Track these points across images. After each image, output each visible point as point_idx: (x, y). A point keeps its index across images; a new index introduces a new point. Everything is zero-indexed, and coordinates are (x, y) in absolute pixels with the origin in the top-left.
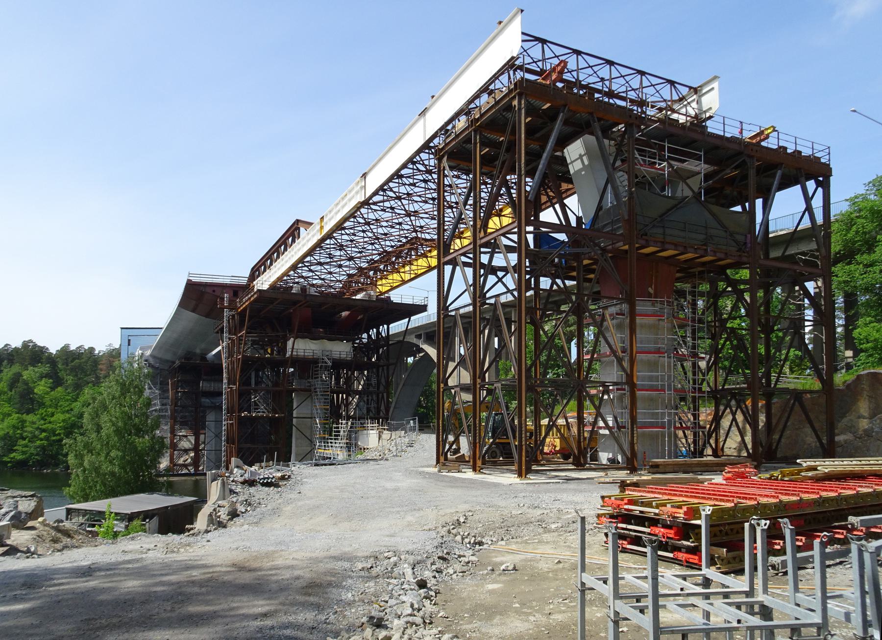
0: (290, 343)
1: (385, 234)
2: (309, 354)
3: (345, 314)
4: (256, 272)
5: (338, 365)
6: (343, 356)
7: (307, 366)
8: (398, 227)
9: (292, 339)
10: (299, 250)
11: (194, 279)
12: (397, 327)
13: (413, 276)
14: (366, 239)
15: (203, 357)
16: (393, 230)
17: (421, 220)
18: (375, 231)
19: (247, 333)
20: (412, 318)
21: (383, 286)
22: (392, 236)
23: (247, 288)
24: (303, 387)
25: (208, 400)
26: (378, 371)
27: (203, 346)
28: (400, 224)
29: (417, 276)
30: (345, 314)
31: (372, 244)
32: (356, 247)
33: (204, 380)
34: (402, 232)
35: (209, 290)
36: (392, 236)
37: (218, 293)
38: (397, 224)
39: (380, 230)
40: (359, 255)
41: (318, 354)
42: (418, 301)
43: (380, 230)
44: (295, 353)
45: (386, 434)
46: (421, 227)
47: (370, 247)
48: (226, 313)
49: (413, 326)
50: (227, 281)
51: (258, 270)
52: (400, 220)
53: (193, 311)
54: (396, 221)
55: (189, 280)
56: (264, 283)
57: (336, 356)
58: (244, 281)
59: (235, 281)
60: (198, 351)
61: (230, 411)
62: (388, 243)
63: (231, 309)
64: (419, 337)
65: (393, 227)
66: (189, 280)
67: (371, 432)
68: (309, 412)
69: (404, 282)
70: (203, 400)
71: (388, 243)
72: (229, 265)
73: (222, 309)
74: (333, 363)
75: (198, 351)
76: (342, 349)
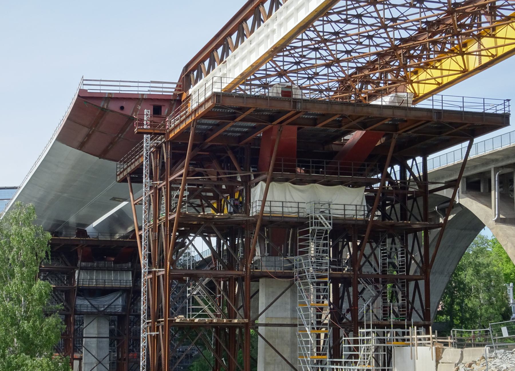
0: (257, 193)
1: (336, 34)
2: (291, 211)
3: (354, 137)
4: (191, 73)
5: (343, 230)
6: (350, 213)
7: (285, 232)
8: (356, 21)
9: (262, 185)
10: (287, 19)
11: (92, 89)
12: (444, 159)
13: (485, 60)
14: (305, 43)
15: (82, 232)
16: (349, 26)
17: (393, 10)
18: (319, 28)
19: (188, 174)
20: (476, 140)
21: (424, 82)
22: (347, 35)
23: (178, 100)
24: (278, 270)
25: (86, 302)
26: (405, 244)
27: (83, 211)
28: (359, 16)
29: (496, 60)
30: (354, 137)
31: (316, 49)
32: (291, 55)
33: (82, 269)
34: (362, 30)
35: (114, 106)
36: (347, 35)
37: (129, 110)
38: (354, 16)
39: (328, 28)
40: (295, 67)
41: (307, 210)
42: (493, 107)
43: (328, 28)
44: (267, 209)
45: (451, 354)
46: (394, 20)
47: (313, 55)
48: (147, 142)
49: (481, 153)
50: (144, 90)
51: (198, 67)
52: (360, 11)
53: (81, 147)
54: (353, 12)
55: (81, 91)
56: (200, 93)
57: (337, 212)
58: (170, 90)
59: (158, 91)
60: (72, 220)
61: (156, 314)
62: (341, 47)
63: (154, 135)
64: (453, 185)
65: (349, 22)
66: (81, 91)
67: (420, 350)
68: (288, 314)
69: (466, 74)
70: (79, 302)
71: (341, 47)
72: (144, 63)
73: (141, 134)
74: (334, 225)
75: (72, 220)
76: (347, 201)
